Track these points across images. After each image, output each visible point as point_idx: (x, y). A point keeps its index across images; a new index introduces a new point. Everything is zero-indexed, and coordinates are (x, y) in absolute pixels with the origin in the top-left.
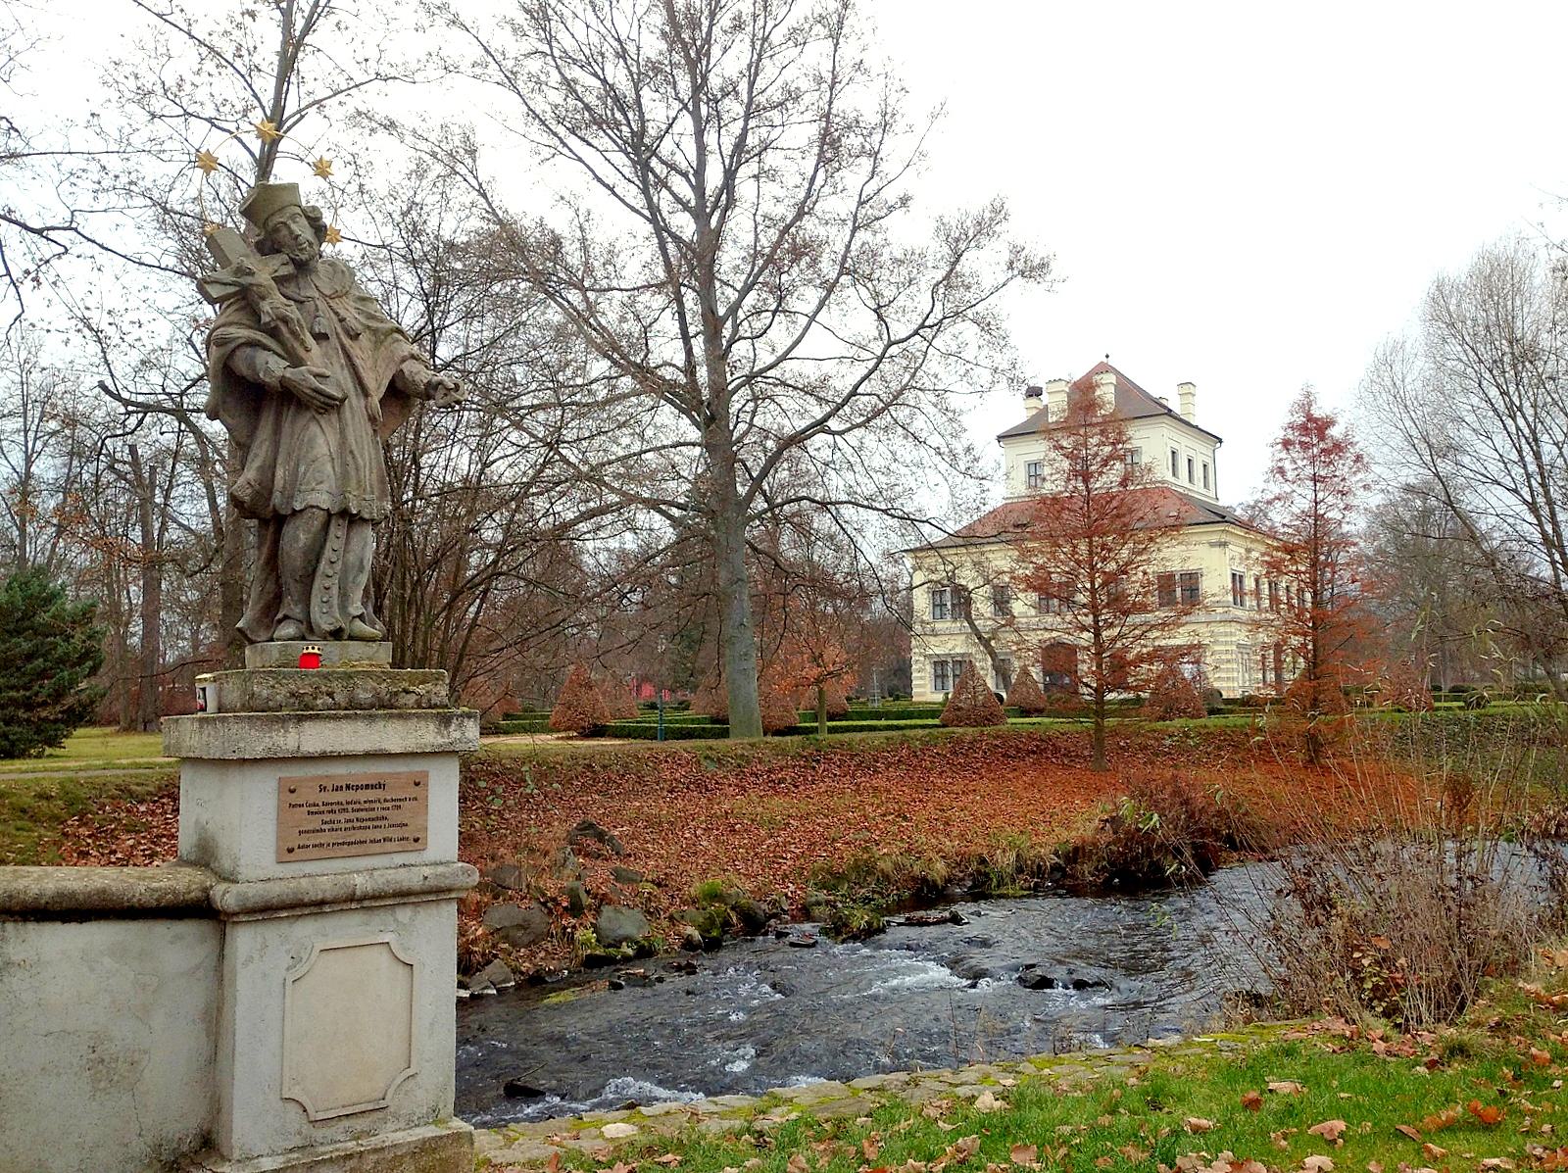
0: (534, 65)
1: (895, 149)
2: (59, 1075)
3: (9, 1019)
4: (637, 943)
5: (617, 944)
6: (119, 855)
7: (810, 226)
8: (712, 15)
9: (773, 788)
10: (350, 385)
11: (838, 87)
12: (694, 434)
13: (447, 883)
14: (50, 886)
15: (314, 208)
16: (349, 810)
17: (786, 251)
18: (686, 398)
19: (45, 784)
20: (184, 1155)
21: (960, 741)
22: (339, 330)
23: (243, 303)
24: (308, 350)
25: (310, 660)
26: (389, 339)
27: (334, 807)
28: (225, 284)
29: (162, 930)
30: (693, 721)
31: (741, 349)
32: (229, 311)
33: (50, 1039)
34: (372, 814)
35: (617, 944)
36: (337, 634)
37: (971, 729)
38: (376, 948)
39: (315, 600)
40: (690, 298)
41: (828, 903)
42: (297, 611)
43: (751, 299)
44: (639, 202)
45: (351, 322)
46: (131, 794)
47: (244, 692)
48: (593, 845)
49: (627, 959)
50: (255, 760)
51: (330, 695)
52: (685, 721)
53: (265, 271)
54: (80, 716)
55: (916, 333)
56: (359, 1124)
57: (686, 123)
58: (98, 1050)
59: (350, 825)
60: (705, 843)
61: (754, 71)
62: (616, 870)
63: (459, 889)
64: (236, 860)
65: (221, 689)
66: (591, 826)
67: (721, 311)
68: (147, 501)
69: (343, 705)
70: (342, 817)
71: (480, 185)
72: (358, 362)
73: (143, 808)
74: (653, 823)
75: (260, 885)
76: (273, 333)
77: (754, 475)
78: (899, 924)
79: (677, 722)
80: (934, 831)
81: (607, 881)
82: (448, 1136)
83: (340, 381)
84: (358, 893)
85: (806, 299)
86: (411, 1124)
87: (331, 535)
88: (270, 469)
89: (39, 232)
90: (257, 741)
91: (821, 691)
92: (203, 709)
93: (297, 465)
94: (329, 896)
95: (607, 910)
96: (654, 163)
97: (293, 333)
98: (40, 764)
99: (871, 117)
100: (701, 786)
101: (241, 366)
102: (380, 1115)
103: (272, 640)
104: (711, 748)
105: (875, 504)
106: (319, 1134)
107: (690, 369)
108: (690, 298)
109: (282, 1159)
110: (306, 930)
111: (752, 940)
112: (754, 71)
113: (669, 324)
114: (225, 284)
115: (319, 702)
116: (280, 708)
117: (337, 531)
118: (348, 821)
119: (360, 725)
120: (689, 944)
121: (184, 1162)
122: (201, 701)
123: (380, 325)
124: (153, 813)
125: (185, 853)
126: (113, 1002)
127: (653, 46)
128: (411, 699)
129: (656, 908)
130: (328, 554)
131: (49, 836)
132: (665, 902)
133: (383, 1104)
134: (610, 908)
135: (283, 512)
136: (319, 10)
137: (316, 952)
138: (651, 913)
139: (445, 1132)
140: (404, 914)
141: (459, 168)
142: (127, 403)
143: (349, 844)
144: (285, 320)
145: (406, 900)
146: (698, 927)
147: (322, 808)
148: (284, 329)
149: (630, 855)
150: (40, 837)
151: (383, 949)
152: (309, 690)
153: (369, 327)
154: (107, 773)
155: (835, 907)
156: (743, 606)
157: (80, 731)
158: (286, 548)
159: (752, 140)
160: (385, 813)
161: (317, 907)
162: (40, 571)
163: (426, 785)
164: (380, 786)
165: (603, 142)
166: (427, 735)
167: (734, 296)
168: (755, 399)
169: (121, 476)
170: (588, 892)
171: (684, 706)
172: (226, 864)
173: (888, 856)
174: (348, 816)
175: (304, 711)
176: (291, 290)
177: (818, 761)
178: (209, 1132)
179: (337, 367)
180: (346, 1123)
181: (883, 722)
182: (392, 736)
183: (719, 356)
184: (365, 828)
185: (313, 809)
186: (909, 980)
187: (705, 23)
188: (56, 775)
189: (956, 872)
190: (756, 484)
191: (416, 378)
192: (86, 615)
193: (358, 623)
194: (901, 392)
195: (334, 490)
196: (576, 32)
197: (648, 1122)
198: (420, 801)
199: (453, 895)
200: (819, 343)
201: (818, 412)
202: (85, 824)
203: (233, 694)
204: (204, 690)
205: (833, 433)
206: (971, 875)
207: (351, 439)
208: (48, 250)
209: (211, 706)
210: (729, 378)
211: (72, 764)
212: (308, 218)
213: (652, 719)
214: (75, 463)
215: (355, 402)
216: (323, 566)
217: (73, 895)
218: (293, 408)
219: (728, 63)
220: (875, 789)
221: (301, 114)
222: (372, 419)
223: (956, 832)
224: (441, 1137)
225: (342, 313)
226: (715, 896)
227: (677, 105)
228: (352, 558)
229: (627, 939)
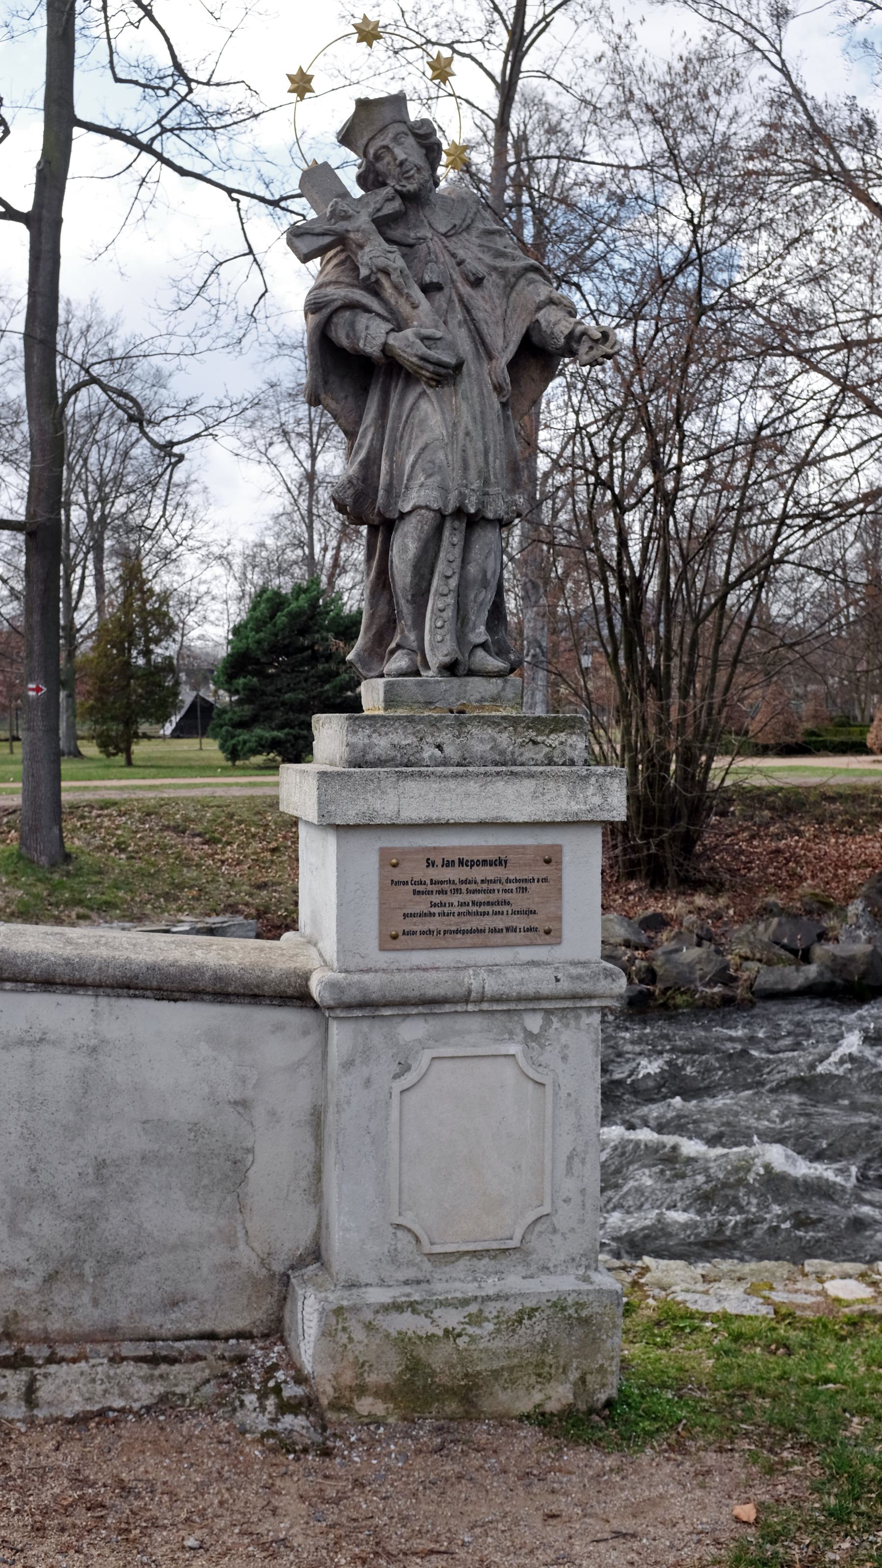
24: (415, 307)
26: (522, 282)
27: (445, 887)
28: (318, 235)
34: (492, 897)
51: (439, 747)
59: (464, 909)
63: (601, 997)
70: (455, 899)
71: (783, 62)
72: (479, 315)
87: (445, 543)
89: (275, 203)
101: (341, 336)
114: (318, 235)
117: (452, 538)
118: (461, 904)
143: (464, 932)
147: (430, 887)
153: (495, 269)
160: (507, 897)
161: (429, 1004)
163: (559, 863)
164: (501, 862)
182: (515, 800)
184: (484, 914)
191: (556, 330)
193: (480, 653)
199: (595, 1003)
212: (416, 136)
221: (545, 21)
225: (461, 253)
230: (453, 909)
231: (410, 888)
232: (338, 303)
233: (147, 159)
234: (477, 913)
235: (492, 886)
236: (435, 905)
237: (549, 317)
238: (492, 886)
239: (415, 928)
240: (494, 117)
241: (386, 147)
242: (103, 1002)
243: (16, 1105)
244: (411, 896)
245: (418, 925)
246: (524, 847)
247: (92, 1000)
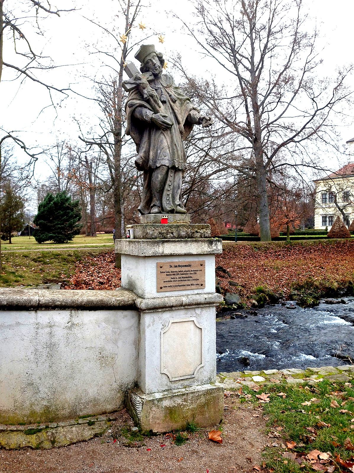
0: (200, 26)
1: (318, 43)
2: (90, 361)
3: (74, 343)
4: (238, 304)
5: (231, 304)
6: (90, 272)
7: (289, 72)
8: (257, 3)
9: (277, 257)
10: (174, 120)
11: (299, 24)
12: (251, 145)
13: (213, 300)
14: (85, 298)
15: (160, 53)
16: (178, 275)
17: (282, 81)
18: (247, 133)
19: (70, 252)
20: (129, 389)
21: (339, 243)
22: (170, 100)
23: (136, 92)
25: (165, 221)
27: (175, 273)
28: (132, 84)
29: (120, 314)
30: (245, 235)
31: (265, 116)
32: (133, 94)
33: (87, 350)
34: (187, 276)
35: (231, 304)
36: (172, 211)
37: (343, 239)
38: (190, 322)
39: (164, 199)
40: (249, 99)
41: (298, 295)
42: (158, 203)
43: (269, 99)
44: (233, 69)
45: (173, 96)
46: (92, 255)
47: (144, 232)
48: (222, 274)
49: (235, 310)
50: (149, 256)
51: (172, 233)
52: (243, 235)
53: (145, 78)
54: (77, 233)
55: (327, 106)
56: (186, 383)
57: (248, 40)
58: (102, 353)
59: (180, 279)
60: (256, 274)
61: (271, 20)
62: (230, 282)
63: (216, 303)
64: (143, 291)
65: (134, 231)
66: (221, 268)
67: (259, 104)
68: (90, 172)
69: (176, 237)
70: (177, 277)
71: (182, 68)
72: (176, 111)
73: (95, 259)
74: (240, 267)
75: (152, 300)
76: (148, 101)
77: (269, 157)
78: (323, 303)
79: (240, 235)
80: (333, 273)
81: (227, 285)
82: (215, 389)
83: (170, 120)
84: (184, 303)
85: (288, 96)
86: (203, 384)
87: (169, 176)
88: (147, 152)
90: (150, 250)
91: (288, 226)
92: (129, 237)
93: (157, 150)
94: (174, 304)
95: (228, 294)
96: (237, 55)
97: (155, 101)
98: (67, 245)
99: (311, 33)
100: (253, 256)
101: (137, 114)
102: (192, 380)
103: (150, 213)
104: (256, 244)
105: (310, 165)
106: (173, 386)
107: (249, 124)
108: (249, 99)
109: (162, 394)
110: (167, 316)
111: (274, 306)
112: (271, 20)
113: (243, 109)
114: (132, 84)
115: (168, 236)
116: (156, 238)
117: (171, 174)
118: (180, 278)
119: (183, 244)
120: (253, 305)
121: (129, 391)
122: (128, 235)
123: (182, 97)
124: (98, 261)
125: (124, 285)
126: (106, 338)
127: (238, 16)
128: (198, 235)
129: (243, 294)
130: (168, 182)
131: (72, 266)
132: (245, 292)
133: (193, 376)
134: (229, 293)
135: (152, 167)
136: (137, 13)
137: (170, 323)
138: (241, 296)
139: (215, 387)
140: (198, 311)
141: (176, 63)
142: (86, 142)
143: (180, 286)
144: (152, 96)
145: (199, 306)
146: (257, 301)
148: (152, 100)
149: (233, 277)
150: (69, 267)
151: (192, 323)
152: (165, 231)
153: (178, 98)
154: (86, 249)
155: (301, 296)
156: (265, 200)
157: (77, 236)
158: (154, 181)
159: (269, 45)
160: (191, 275)
162: (64, 192)
163: (204, 265)
164: (189, 266)
165: (221, 50)
166: (205, 248)
167: (262, 99)
168: (269, 132)
169: (83, 165)
170: (222, 288)
171: (241, 230)
172: (140, 292)
173: (317, 280)
174: (179, 276)
175: (164, 239)
176: (153, 85)
177: (291, 249)
178: (137, 382)
179: (169, 113)
180: (181, 382)
181: (306, 236)
182: (193, 248)
183: (258, 119)
184: (185, 280)
185: (168, 274)
186: (326, 322)
187: (255, 6)
188: (72, 249)
189: (341, 286)
190: (270, 159)
191: (195, 117)
192: (76, 205)
193: (179, 207)
194: (319, 127)
195: (170, 159)
196: (214, 12)
197: (268, 377)
198: (203, 271)
200: (289, 113)
201: (291, 135)
202: (81, 263)
203: (139, 233)
204: (129, 231)
205: (296, 142)
206: (346, 287)
207: (175, 140)
208: (63, 96)
209: (132, 236)
210: (261, 126)
211: (75, 245)
212: (158, 57)
213: (233, 235)
214: (71, 162)
215: (176, 126)
216: (167, 187)
217: (92, 302)
218: (154, 130)
219: (262, 20)
220: (311, 258)
222: (181, 133)
223: (340, 273)
224: (213, 389)
225: (170, 93)
226: (260, 291)
227: (246, 35)
228: (176, 184)
229: (235, 303)
230: (177, 280)
231: (166, 274)
232: (138, 105)
233: (24, 75)
234: (183, 280)
235: (187, 273)
236: (172, 278)
237: (193, 113)
238: (187, 273)
239: (167, 285)
240: (119, 72)
241: (150, 59)
242: (73, 312)
243: (45, 346)
244: (166, 276)
245: (168, 284)
246: (195, 261)
247: (70, 311)
